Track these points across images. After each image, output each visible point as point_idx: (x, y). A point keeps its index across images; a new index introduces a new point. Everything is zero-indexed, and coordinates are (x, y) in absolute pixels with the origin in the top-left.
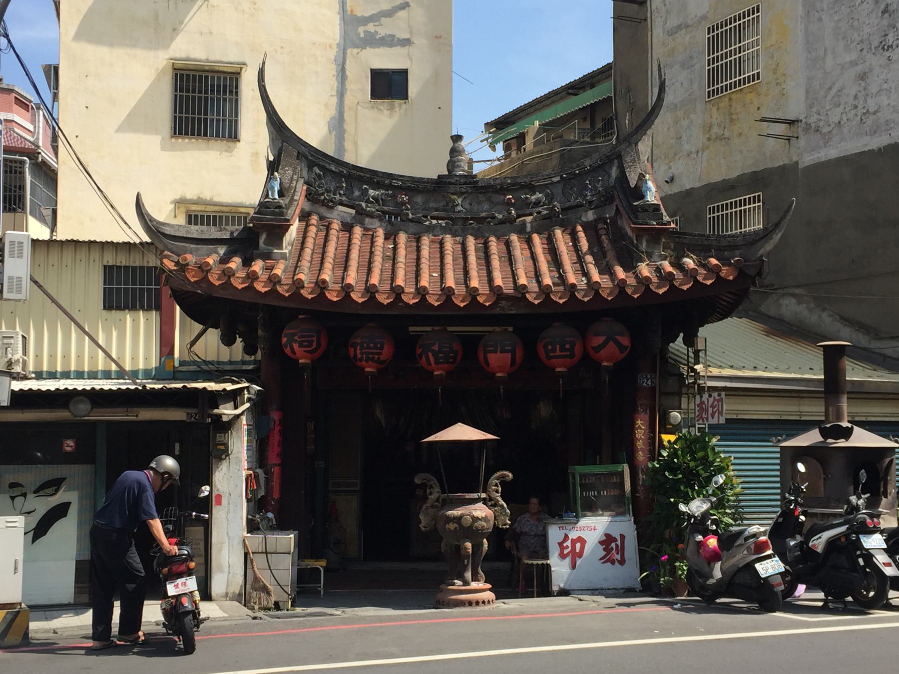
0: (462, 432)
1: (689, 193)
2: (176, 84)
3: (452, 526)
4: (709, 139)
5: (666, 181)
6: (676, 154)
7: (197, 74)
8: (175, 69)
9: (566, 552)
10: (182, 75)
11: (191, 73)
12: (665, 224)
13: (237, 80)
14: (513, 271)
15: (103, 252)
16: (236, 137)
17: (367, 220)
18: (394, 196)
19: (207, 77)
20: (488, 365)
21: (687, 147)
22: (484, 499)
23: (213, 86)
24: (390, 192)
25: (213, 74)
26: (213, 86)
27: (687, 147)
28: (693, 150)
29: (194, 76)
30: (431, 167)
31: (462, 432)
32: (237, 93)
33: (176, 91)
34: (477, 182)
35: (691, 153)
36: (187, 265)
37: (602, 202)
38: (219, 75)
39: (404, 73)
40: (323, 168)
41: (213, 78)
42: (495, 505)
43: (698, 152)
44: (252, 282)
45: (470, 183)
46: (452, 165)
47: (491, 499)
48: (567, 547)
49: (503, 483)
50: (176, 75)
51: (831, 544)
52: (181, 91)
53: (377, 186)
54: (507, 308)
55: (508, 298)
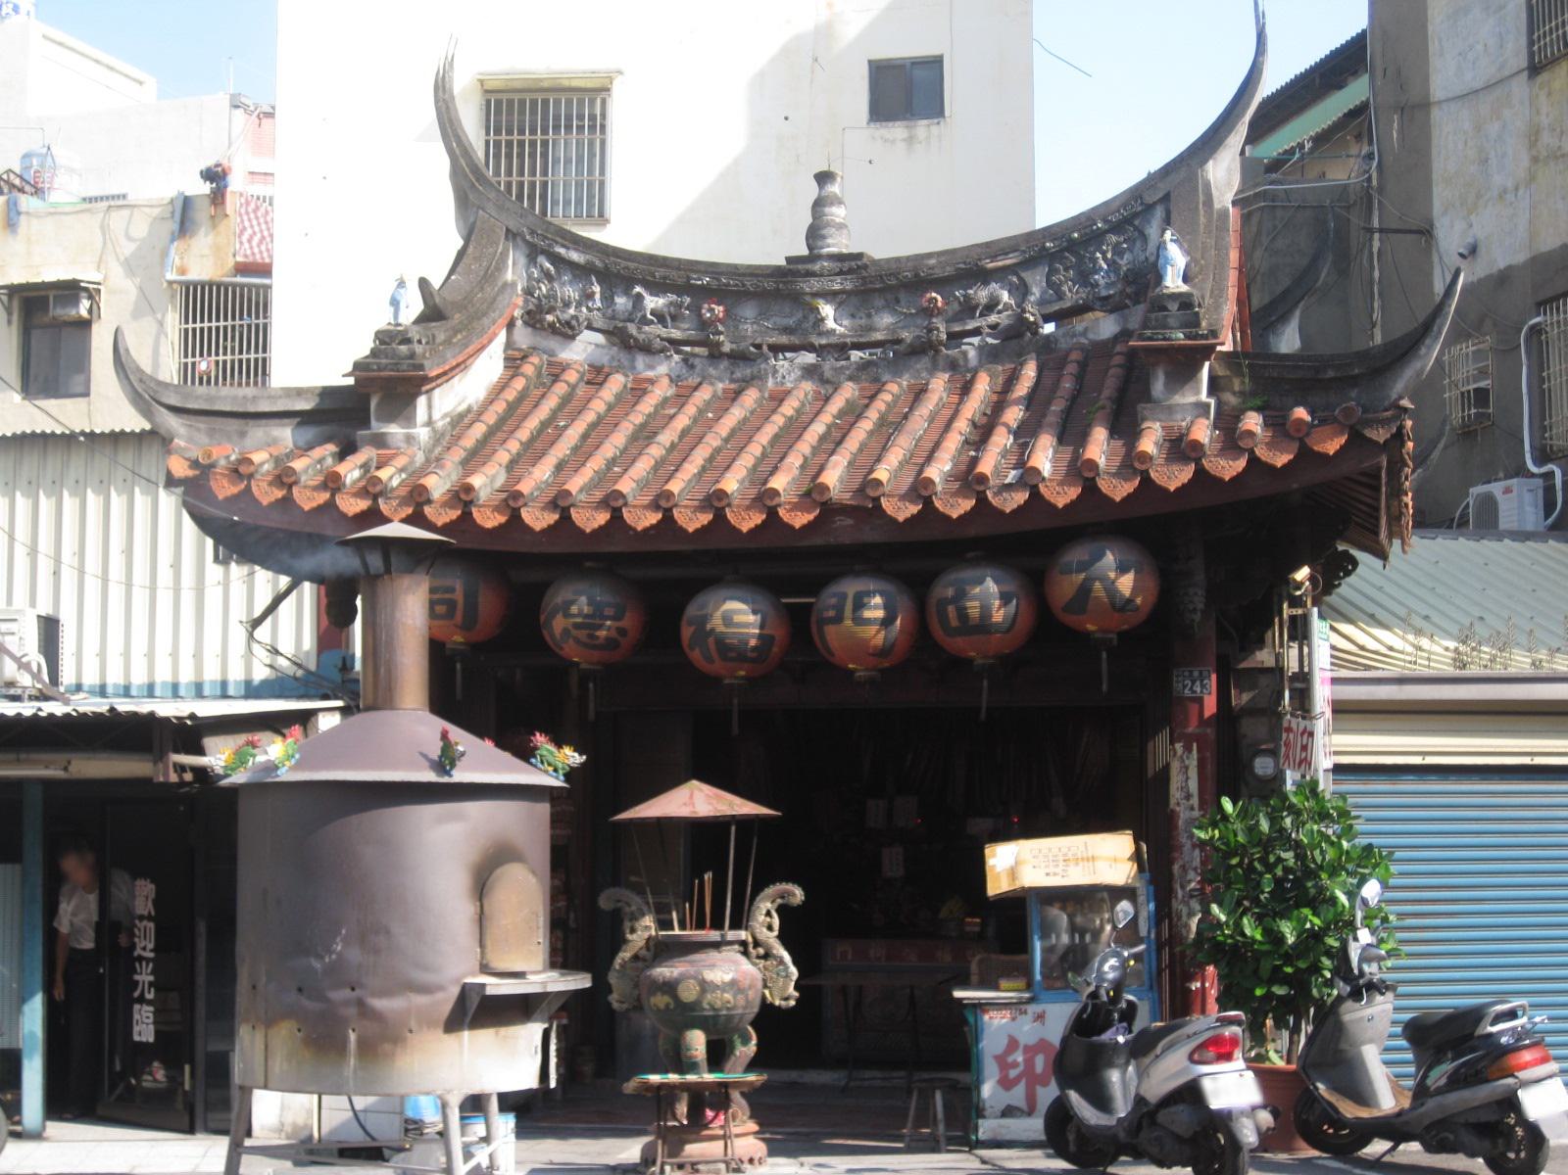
0: (695, 800)
1: (1503, 279)
2: (488, 120)
3: (660, 1000)
4: (1535, 160)
5: (1461, 255)
6: (1479, 196)
7: (504, 97)
8: (487, 91)
9: (1013, 1073)
10: (499, 103)
11: (516, 97)
12: (1204, 337)
13: (604, 102)
14: (880, 455)
15: (140, 455)
16: (601, 215)
17: (641, 361)
18: (696, 309)
19: (546, 102)
20: (832, 654)
21: (1498, 180)
22: (744, 944)
23: (557, 118)
24: (687, 300)
25: (556, 95)
26: (557, 118)
27: (1498, 180)
28: (1510, 185)
29: (522, 102)
30: (770, 243)
31: (695, 800)
32: (603, 127)
33: (488, 133)
34: (865, 267)
35: (1505, 191)
36: (212, 466)
37: (1128, 296)
38: (569, 95)
39: (935, 63)
40: (556, 260)
41: (557, 102)
42: (766, 956)
43: (1517, 189)
44: (333, 496)
45: (850, 271)
46: (814, 234)
47: (757, 944)
48: (1015, 1065)
49: (784, 911)
50: (488, 102)
51: (1288, 1021)
52: (498, 132)
53: (656, 288)
54: (844, 533)
55: (843, 509)
